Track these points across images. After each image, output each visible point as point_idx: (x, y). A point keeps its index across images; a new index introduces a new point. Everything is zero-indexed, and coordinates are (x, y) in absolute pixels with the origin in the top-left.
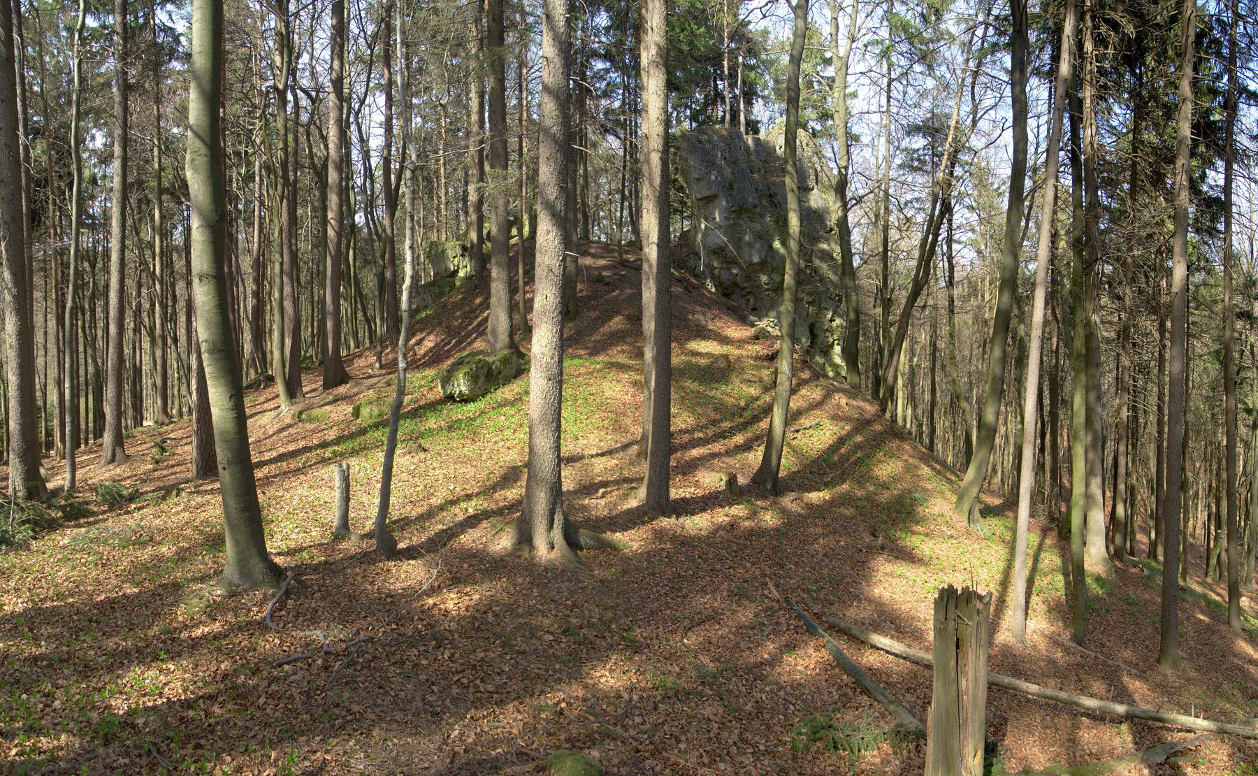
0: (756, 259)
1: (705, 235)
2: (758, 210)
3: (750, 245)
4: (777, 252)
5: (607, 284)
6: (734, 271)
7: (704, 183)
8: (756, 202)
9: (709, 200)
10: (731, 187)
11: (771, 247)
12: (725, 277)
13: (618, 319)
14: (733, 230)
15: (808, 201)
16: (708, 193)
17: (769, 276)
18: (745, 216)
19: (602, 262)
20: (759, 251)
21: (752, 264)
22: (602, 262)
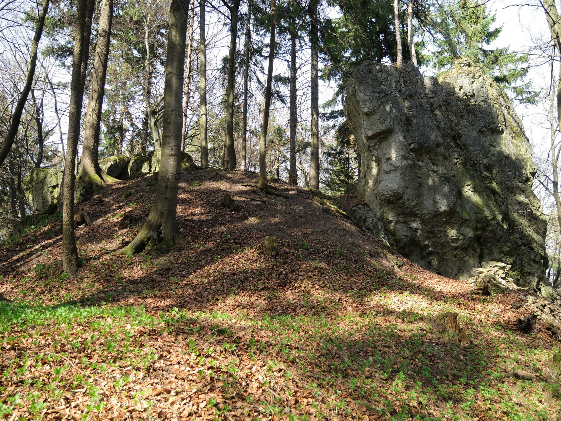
0: (443, 207)
1: (377, 182)
2: (441, 149)
3: (434, 189)
4: (468, 199)
5: (237, 209)
6: (414, 225)
7: (376, 117)
8: (440, 139)
9: (382, 137)
10: (408, 121)
11: (460, 193)
12: (402, 231)
13: (250, 253)
14: (412, 172)
15: (499, 145)
16: (381, 128)
17: (458, 230)
18: (426, 157)
19: (240, 187)
20: (446, 196)
21: (437, 214)
22: (240, 187)
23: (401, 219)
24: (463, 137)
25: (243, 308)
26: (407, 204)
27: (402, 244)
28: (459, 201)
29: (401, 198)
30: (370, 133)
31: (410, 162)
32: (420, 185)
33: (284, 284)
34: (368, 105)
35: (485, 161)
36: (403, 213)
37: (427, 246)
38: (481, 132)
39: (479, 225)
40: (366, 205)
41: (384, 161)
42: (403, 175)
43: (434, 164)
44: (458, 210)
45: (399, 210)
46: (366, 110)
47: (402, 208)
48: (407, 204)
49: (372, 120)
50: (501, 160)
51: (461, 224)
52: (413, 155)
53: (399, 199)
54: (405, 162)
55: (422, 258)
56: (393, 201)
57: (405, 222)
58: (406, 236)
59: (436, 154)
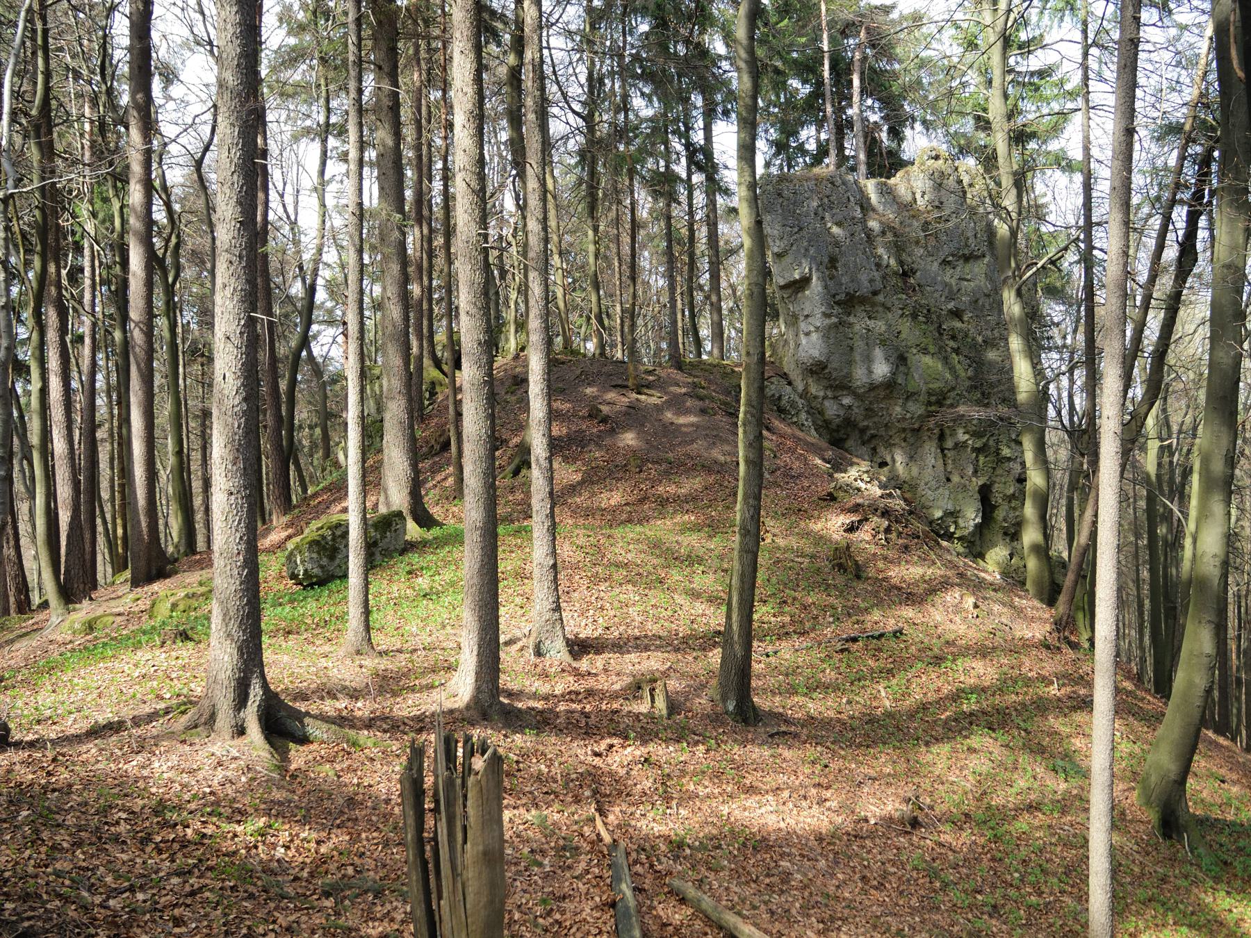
2: (880, 298)
14: (837, 332)
23: (829, 394)
24: (918, 274)
25: (774, 694)
26: (834, 375)
27: (834, 426)
28: (902, 368)
29: (826, 367)
30: (782, 282)
31: (834, 320)
32: (852, 349)
33: (808, 412)
34: (778, 243)
35: (951, 305)
36: (831, 386)
37: (867, 427)
38: (945, 262)
39: (933, 399)
40: (785, 376)
41: (802, 318)
42: (826, 337)
43: (870, 318)
44: (899, 381)
45: (825, 383)
46: (776, 250)
47: (829, 379)
48: (834, 375)
49: (784, 263)
50: (976, 301)
51: (907, 398)
52: (837, 310)
53: (823, 369)
54: (827, 321)
55: (863, 444)
56: (817, 370)
57: (835, 398)
58: (838, 416)
59: (873, 305)
